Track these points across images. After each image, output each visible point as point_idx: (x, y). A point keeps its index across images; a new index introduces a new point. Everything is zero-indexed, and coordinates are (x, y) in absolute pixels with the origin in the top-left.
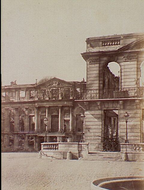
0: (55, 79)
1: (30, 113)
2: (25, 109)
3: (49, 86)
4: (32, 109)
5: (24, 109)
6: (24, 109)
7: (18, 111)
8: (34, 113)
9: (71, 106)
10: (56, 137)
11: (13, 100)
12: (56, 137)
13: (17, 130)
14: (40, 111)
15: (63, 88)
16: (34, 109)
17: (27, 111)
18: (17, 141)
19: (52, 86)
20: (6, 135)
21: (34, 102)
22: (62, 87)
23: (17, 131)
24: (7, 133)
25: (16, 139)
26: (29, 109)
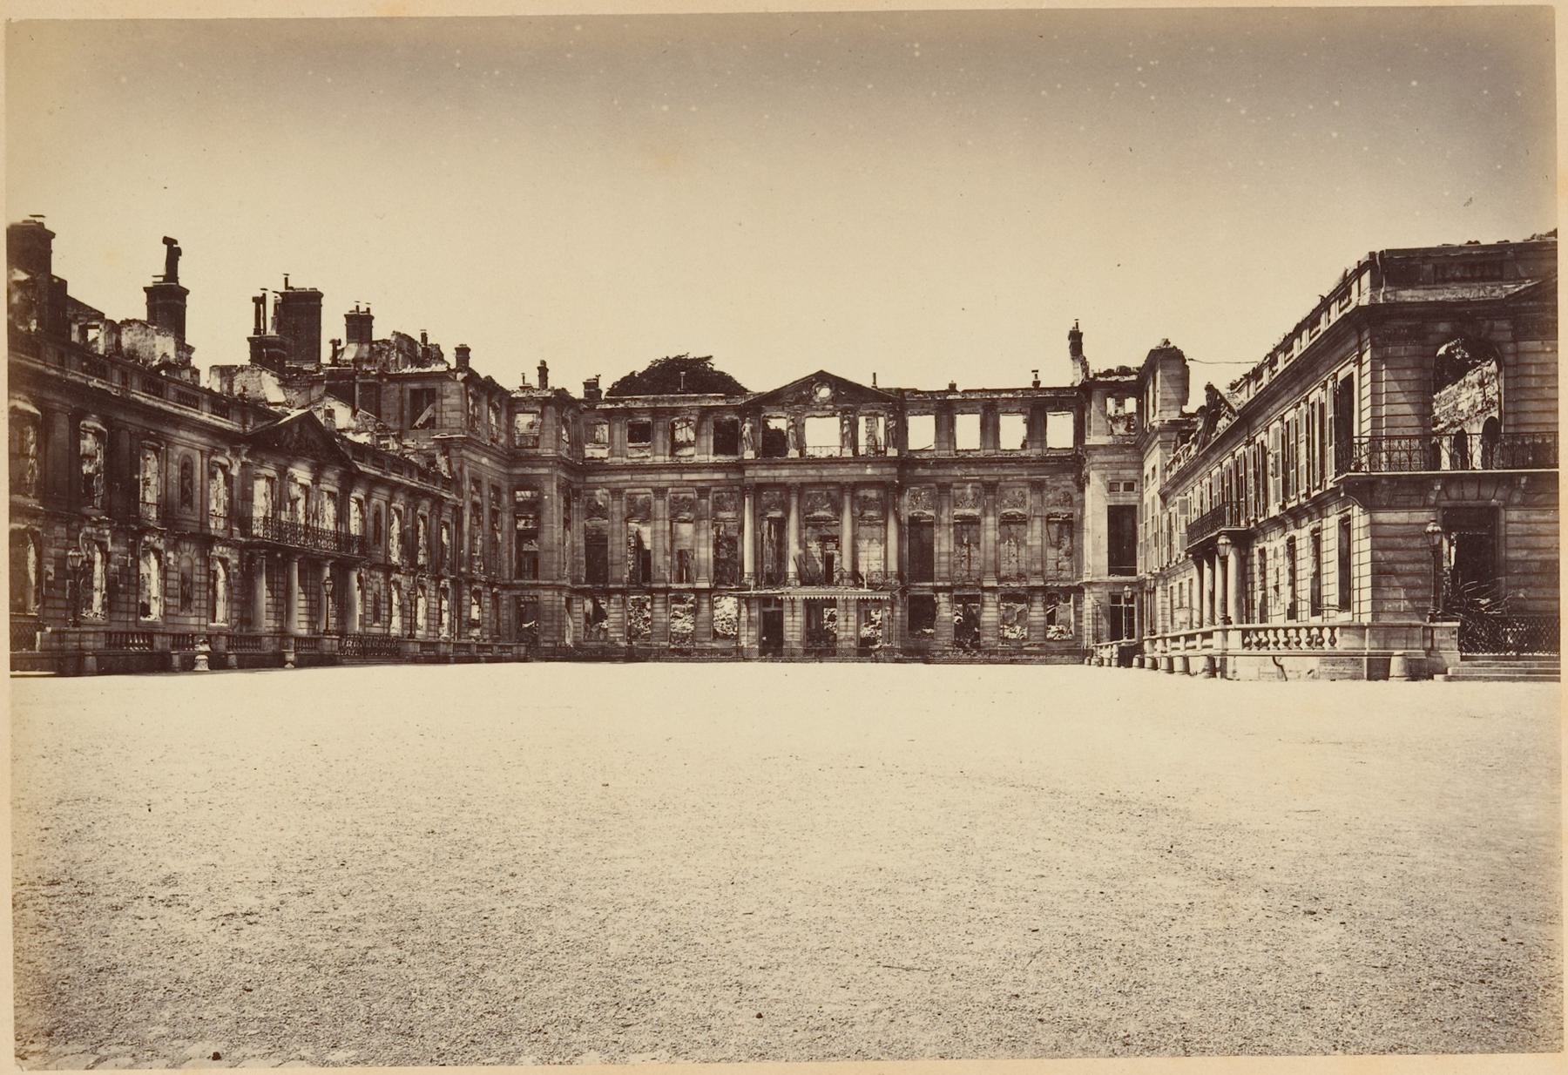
0: (822, 378)
23: (664, 581)
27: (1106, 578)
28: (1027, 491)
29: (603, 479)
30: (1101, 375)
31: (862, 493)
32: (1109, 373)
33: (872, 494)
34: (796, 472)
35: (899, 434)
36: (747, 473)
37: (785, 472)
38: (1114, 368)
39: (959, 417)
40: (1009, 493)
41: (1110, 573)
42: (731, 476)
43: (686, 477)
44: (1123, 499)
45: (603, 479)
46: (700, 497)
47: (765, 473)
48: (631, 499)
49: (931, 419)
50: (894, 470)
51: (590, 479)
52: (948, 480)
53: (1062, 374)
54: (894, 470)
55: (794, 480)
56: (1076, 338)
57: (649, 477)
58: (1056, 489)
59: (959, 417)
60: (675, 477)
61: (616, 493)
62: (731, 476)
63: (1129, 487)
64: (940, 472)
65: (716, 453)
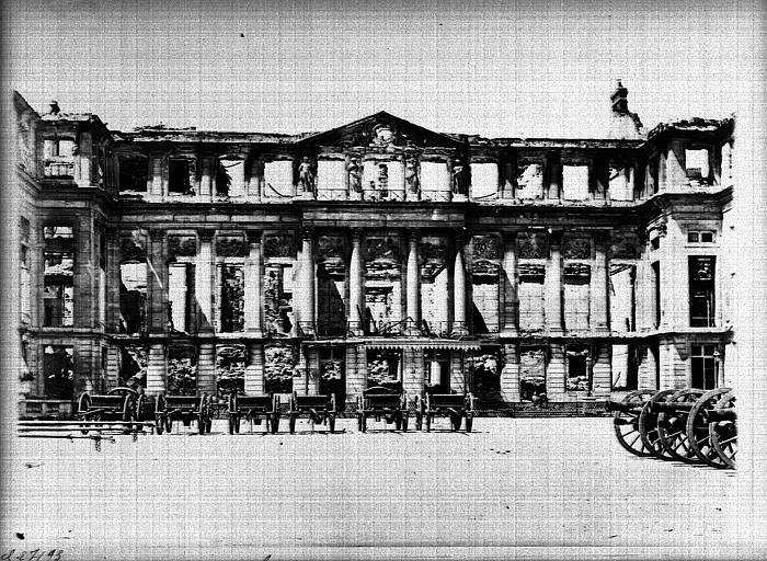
0: (384, 119)
20: (159, 346)
27: (688, 329)
28: (592, 242)
29: (140, 219)
30: (678, 124)
31: (425, 240)
32: (684, 123)
33: (435, 241)
34: (358, 216)
35: (463, 182)
36: (307, 216)
37: (346, 216)
38: (689, 119)
39: (566, 169)
40: (573, 243)
41: (693, 323)
42: (285, 219)
43: (235, 218)
44: (701, 249)
45: (140, 219)
46: (251, 241)
47: (325, 216)
48: (173, 241)
49: (584, 170)
50: (462, 217)
51: (126, 218)
52: (513, 229)
53: (606, 127)
54: (462, 217)
55: (356, 224)
56: (622, 92)
57: (192, 218)
58: (620, 240)
59: (566, 169)
60: (224, 218)
61: (156, 235)
62: (285, 219)
63: (708, 238)
64: (505, 221)
65: (693, 387)
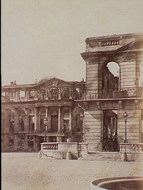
0: (54, 79)
1: (30, 113)
2: (25, 109)
3: (48, 86)
4: (32, 109)
5: (23, 109)
6: (23, 109)
7: (18, 111)
8: (34, 113)
9: (70, 106)
10: (56, 137)
11: (13, 100)
12: (56, 137)
13: (17, 130)
14: (40, 111)
15: (63, 88)
16: (34, 109)
17: (27, 111)
18: (17, 141)
19: (52, 86)
20: (6, 135)
21: (34, 102)
22: (62, 87)
23: (17, 131)
24: (7, 133)
25: (15, 139)
26: (29, 109)
